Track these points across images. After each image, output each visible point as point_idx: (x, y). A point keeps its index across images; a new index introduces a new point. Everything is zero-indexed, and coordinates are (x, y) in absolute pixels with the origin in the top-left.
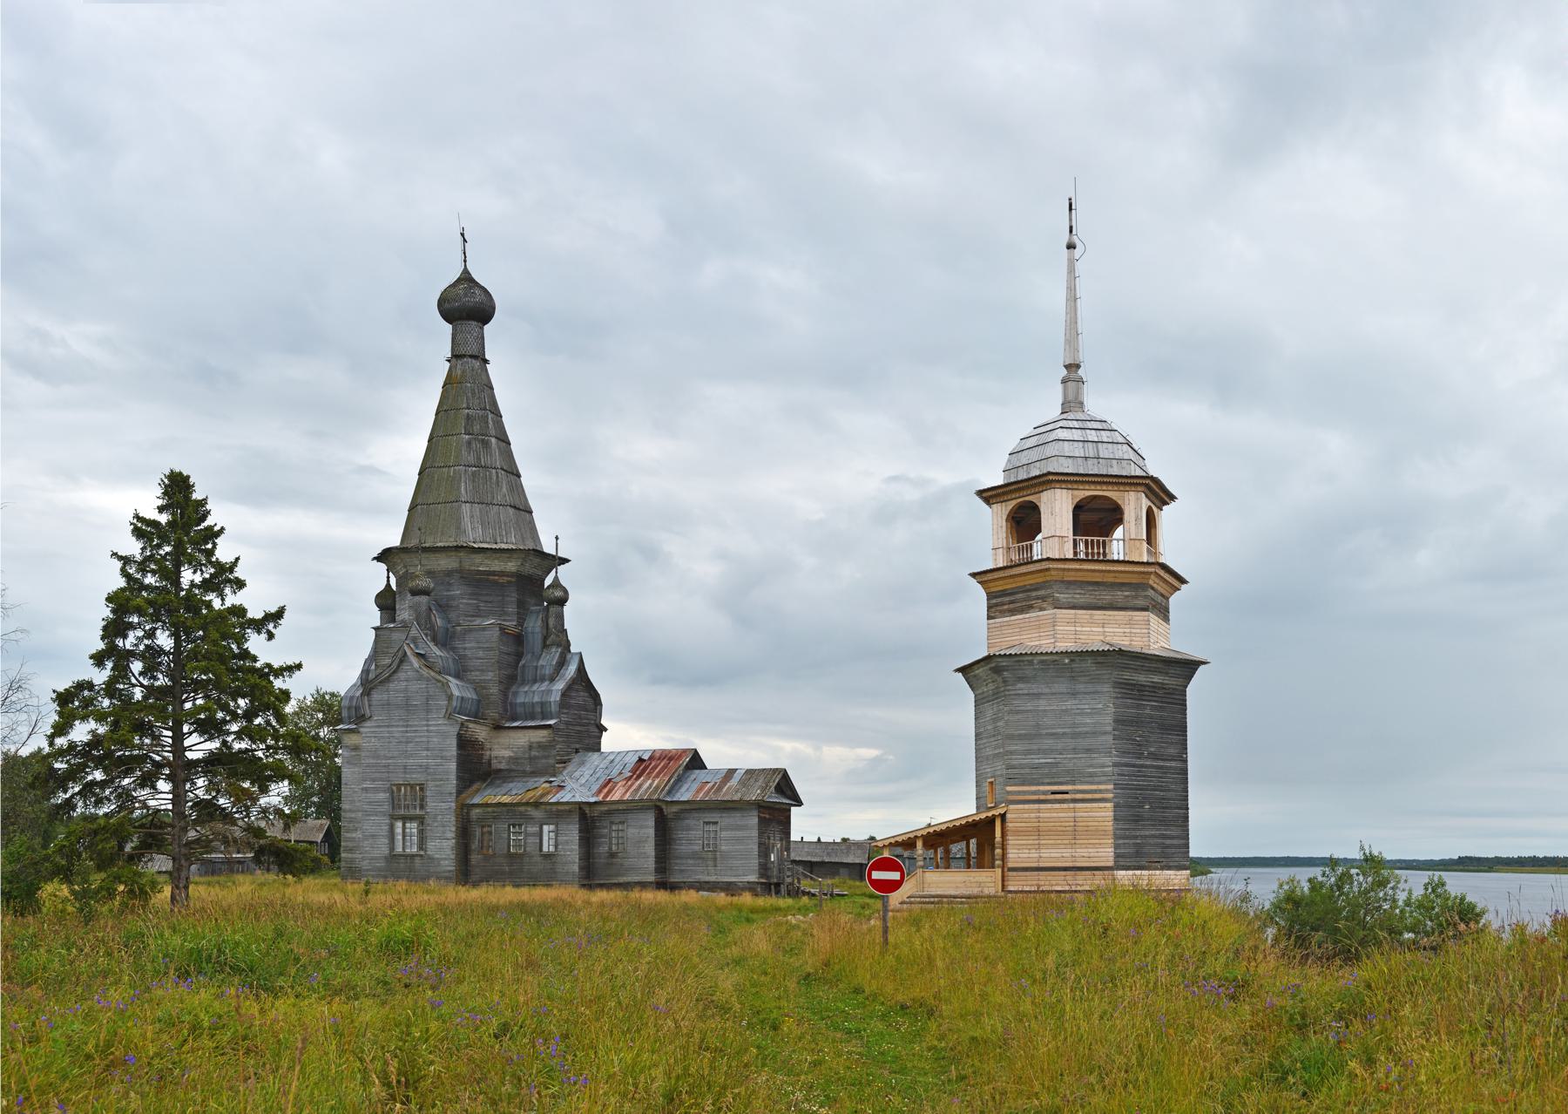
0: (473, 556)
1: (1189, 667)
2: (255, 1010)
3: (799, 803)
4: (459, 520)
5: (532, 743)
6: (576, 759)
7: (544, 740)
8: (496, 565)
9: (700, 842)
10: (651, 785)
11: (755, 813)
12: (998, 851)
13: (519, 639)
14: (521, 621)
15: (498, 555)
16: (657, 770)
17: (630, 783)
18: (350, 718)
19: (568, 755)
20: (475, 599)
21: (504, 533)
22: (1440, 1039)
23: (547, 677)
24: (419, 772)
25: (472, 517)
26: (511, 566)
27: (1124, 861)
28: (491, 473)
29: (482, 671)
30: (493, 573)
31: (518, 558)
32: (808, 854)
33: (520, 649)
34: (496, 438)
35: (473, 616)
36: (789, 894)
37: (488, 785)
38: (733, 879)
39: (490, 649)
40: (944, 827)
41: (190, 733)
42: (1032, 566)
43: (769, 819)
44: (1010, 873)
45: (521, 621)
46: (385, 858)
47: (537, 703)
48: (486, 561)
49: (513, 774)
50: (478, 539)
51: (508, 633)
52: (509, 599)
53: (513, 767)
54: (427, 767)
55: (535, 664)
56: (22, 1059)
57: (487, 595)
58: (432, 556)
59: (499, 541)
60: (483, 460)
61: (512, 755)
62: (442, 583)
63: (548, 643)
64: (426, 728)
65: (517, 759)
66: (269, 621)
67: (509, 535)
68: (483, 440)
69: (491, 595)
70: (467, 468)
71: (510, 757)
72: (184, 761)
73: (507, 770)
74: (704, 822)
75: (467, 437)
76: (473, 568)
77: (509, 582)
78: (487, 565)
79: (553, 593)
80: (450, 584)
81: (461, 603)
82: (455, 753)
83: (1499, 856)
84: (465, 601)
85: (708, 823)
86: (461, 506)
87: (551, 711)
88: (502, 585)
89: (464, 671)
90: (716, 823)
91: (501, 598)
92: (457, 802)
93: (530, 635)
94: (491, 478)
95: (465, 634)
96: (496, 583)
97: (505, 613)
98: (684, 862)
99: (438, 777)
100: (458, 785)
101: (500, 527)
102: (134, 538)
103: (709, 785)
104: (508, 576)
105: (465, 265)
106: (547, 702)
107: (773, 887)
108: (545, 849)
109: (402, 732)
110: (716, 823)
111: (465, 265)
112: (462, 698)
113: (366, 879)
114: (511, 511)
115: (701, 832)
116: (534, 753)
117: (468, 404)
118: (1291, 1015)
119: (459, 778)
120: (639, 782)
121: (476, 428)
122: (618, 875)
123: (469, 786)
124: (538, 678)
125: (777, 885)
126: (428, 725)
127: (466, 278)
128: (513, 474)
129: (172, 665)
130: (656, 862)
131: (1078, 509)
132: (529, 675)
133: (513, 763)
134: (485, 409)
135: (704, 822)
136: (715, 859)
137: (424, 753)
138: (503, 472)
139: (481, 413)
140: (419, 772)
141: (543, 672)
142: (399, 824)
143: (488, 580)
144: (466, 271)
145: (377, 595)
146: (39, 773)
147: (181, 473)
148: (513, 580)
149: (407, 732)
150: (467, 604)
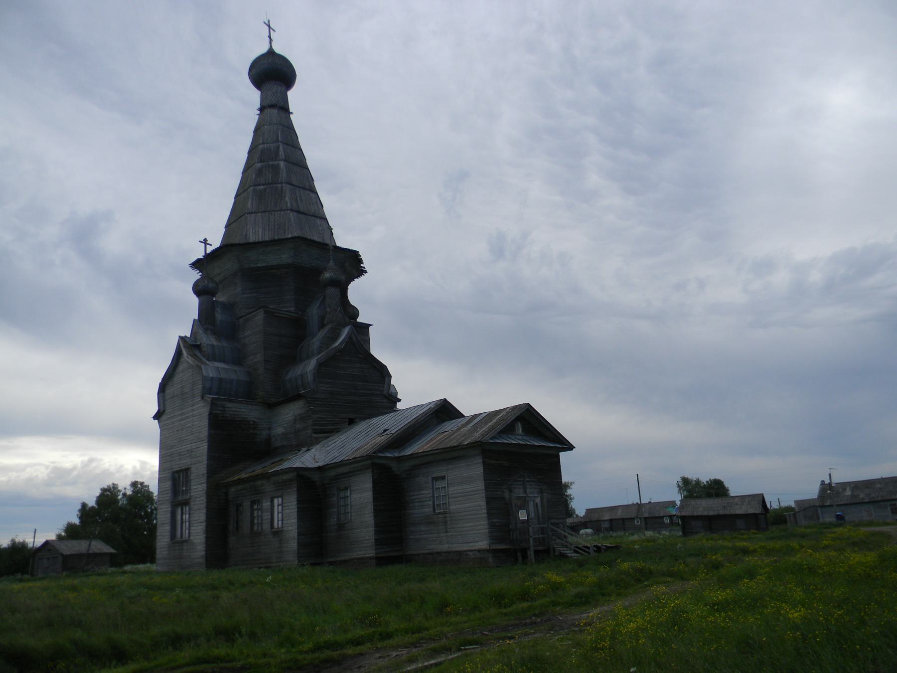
1: (575, 448)
2: (682, 567)
9: (431, 503)
11: (479, 460)
30: (272, 267)
34: (285, 161)
36: (320, 347)
37: (182, 495)
40: (176, 516)
42: (277, 514)
44: (184, 537)
46: (326, 270)
54: (191, 451)
56: (444, 641)
63: (325, 322)
70: (256, 187)
72: (701, 487)
74: (433, 478)
76: (252, 266)
79: (155, 497)
83: (297, 77)
85: (436, 479)
87: (308, 382)
90: (443, 478)
105: (271, 46)
107: (519, 554)
108: (276, 526)
110: (443, 478)
111: (271, 46)
112: (221, 380)
113: (740, 503)
115: (430, 491)
116: (298, 426)
125: (524, 552)
128: (304, 189)
130: (376, 531)
131: (528, 409)
134: (277, 141)
135: (433, 478)
136: (445, 523)
145: (528, 404)
147: (96, 501)
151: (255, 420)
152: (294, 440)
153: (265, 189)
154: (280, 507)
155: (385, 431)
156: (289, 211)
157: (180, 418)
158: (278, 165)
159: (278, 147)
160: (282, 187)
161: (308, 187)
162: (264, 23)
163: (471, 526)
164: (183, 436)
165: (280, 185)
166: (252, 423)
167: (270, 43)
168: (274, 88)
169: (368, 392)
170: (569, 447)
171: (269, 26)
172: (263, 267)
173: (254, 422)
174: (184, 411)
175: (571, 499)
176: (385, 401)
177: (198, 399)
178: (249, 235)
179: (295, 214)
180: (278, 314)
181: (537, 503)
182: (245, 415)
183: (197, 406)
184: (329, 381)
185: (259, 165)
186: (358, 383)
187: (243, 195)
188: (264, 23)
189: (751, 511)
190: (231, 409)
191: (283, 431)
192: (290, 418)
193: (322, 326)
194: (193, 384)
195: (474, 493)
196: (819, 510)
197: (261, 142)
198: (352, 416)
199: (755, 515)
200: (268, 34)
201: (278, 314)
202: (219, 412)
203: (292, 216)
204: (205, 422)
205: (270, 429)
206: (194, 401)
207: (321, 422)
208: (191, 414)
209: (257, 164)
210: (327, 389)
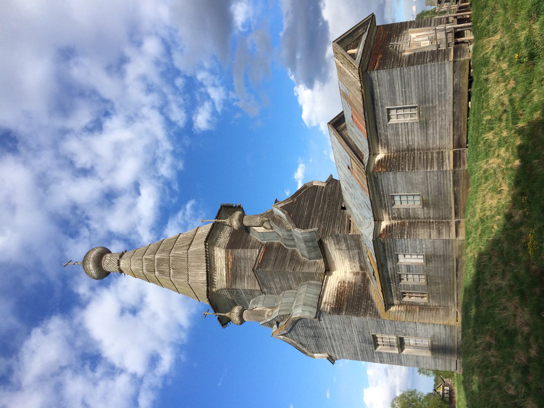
3: (372, 17)
7: (333, 242)
12: (416, 86)
18: (407, 289)
20: (244, 278)
22: (373, 313)
27: (403, 337)
30: (227, 265)
41: (434, 330)
52: (242, 254)
66: (296, 324)
71: (350, 261)
77: (232, 254)
78: (222, 270)
88: (234, 259)
102: (334, 273)
104: (228, 255)
106: (303, 239)
107: (459, 40)
109: (335, 341)
117: (141, 270)
118: (506, 168)
129: (530, 236)
146: (468, 334)
147: (298, 167)
148: (230, 251)
150: (248, 283)
152: (355, 250)
153: (173, 269)
155: (349, 168)
156: (189, 251)
157: (333, 342)
158: (158, 259)
159: (146, 259)
160: (172, 256)
161: (175, 240)
164: (347, 339)
165: (171, 258)
166: (340, 284)
169: (322, 196)
170: (372, 17)
173: (339, 283)
174: (327, 336)
175: (435, 358)
178: (203, 281)
179: (191, 247)
180: (260, 260)
181: (416, 36)
182: (333, 288)
183: (324, 325)
185: (156, 273)
187: (177, 286)
190: (328, 298)
191: (347, 260)
192: (338, 254)
194: (307, 327)
195: (403, 79)
198: (339, 207)
202: (329, 306)
203: (192, 249)
206: (320, 327)
207: (342, 228)
208: (329, 330)
209: (156, 275)
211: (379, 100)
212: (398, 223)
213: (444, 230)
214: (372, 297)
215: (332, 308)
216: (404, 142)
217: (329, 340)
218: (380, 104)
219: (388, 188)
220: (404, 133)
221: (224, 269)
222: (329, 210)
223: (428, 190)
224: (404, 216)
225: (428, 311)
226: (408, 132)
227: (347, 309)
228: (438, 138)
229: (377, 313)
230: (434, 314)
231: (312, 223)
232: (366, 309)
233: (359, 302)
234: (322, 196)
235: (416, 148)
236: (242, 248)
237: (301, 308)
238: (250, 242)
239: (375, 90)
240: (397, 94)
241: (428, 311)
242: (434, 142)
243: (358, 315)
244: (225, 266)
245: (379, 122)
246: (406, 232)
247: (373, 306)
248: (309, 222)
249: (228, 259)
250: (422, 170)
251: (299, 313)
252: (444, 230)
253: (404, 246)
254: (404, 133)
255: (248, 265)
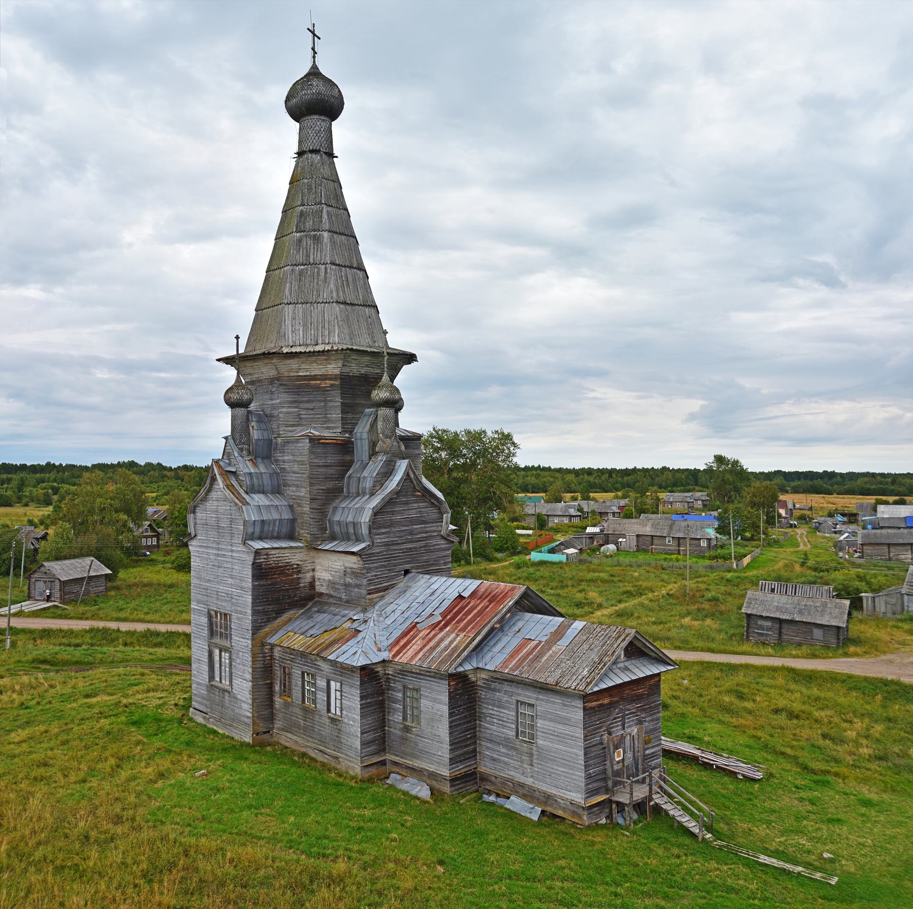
0: (288, 362)
4: (281, 322)
5: (346, 568)
6: (402, 583)
8: (316, 369)
10: (451, 642)
11: (580, 704)
13: (346, 447)
14: (349, 426)
15: (314, 358)
16: (470, 617)
17: (433, 633)
19: (392, 578)
20: (296, 407)
21: (327, 332)
23: (367, 491)
24: (226, 601)
25: (294, 319)
26: (333, 368)
28: (319, 269)
29: (297, 486)
30: (314, 378)
31: (338, 359)
32: (778, 609)
33: (348, 458)
34: (329, 231)
35: (293, 426)
38: (553, 791)
39: (301, 463)
43: (611, 703)
45: (349, 426)
47: (350, 522)
48: (303, 366)
49: (331, 600)
50: (298, 343)
51: (322, 443)
53: (332, 593)
55: (358, 476)
57: (308, 402)
58: (248, 364)
59: (320, 341)
60: (312, 256)
61: (331, 578)
62: (267, 392)
63: (377, 449)
64: (230, 554)
65: (334, 583)
67: (332, 334)
68: (315, 236)
69: (313, 401)
70: (295, 267)
71: (329, 581)
73: (327, 594)
75: (298, 234)
76: (292, 374)
77: (332, 385)
80: (272, 393)
81: (281, 412)
82: (250, 585)
84: (285, 410)
86: (283, 308)
88: (324, 390)
89: (284, 486)
91: (323, 404)
92: (253, 639)
93: (359, 441)
94: (318, 275)
95: (284, 446)
96: (318, 388)
97: (329, 420)
98: (495, 748)
99: (239, 609)
100: (254, 622)
101: (323, 327)
103: (534, 643)
104: (331, 379)
105: (314, 62)
106: (358, 523)
111: (314, 62)
112: (263, 522)
114: (337, 308)
116: (348, 580)
119: (254, 612)
120: (442, 633)
121: (309, 224)
122: (413, 756)
123: (275, 618)
124: (360, 492)
126: (232, 551)
127: (314, 73)
128: (351, 267)
132: (353, 490)
133: (332, 588)
137: (230, 581)
138: (334, 267)
139: (315, 208)
140: (226, 601)
141: (364, 485)
142: (217, 652)
143: (308, 385)
144: (314, 66)
149: (218, 555)
150: (288, 413)
151: (299, 563)
154: (338, 693)
162: (308, 29)
163: (563, 772)
166: (295, 566)
167: (314, 57)
168: (315, 121)
169: (424, 535)
171: (313, 32)
172: (305, 376)
173: (297, 565)
176: (443, 542)
177: (238, 539)
179: (342, 306)
184: (384, 531)
186: (415, 527)
188: (308, 29)
189: (834, 623)
193: (373, 453)
196: (906, 597)
197: (299, 203)
198: (407, 567)
199: (838, 628)
200: (311, 46)
201: (323, 441)
204: (248, 572)
205: (313, 570)
210: (384, 540)
211: (546, 698)
212: (382, 686)
213: (375, 747)
214: (281, 617)
215: (261, 566)
216: (491, 712)
217: (214, 545)
218: (541, 697)
219: (429, 688)
220: (502, 715)
221: (308, 374)
222: (403, 552)
223: (425, 738)
224: (392, 694)
225: (268, 695)
226: (503, 721)
227: (263, 585)
228: (494, 756)
229: (259, 630)
230: (264, 704)
231: (383, 533)
232: (264, 612)
233: (272, 601)
234: (424, 535)
235: (482, 723)
236: (342, 403)
237: (257, 519)
238: (353, 413)
239: (558, 697)
240: (552, 724)
241: (268, 695)
242: (488, 748)
243: (254, 603)
244: (313, 374)
245: (518, 688)
246: (369, 701)
247: (269, 621)
248: (385, 528)
249: (325, 379)
250: (445, 772)
251: (250, 516)
252: (375, 747)
253: (350, 696)
254: (502, 715)
255: (318, 414)
